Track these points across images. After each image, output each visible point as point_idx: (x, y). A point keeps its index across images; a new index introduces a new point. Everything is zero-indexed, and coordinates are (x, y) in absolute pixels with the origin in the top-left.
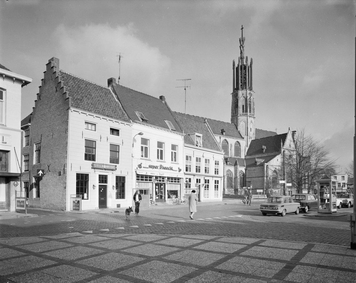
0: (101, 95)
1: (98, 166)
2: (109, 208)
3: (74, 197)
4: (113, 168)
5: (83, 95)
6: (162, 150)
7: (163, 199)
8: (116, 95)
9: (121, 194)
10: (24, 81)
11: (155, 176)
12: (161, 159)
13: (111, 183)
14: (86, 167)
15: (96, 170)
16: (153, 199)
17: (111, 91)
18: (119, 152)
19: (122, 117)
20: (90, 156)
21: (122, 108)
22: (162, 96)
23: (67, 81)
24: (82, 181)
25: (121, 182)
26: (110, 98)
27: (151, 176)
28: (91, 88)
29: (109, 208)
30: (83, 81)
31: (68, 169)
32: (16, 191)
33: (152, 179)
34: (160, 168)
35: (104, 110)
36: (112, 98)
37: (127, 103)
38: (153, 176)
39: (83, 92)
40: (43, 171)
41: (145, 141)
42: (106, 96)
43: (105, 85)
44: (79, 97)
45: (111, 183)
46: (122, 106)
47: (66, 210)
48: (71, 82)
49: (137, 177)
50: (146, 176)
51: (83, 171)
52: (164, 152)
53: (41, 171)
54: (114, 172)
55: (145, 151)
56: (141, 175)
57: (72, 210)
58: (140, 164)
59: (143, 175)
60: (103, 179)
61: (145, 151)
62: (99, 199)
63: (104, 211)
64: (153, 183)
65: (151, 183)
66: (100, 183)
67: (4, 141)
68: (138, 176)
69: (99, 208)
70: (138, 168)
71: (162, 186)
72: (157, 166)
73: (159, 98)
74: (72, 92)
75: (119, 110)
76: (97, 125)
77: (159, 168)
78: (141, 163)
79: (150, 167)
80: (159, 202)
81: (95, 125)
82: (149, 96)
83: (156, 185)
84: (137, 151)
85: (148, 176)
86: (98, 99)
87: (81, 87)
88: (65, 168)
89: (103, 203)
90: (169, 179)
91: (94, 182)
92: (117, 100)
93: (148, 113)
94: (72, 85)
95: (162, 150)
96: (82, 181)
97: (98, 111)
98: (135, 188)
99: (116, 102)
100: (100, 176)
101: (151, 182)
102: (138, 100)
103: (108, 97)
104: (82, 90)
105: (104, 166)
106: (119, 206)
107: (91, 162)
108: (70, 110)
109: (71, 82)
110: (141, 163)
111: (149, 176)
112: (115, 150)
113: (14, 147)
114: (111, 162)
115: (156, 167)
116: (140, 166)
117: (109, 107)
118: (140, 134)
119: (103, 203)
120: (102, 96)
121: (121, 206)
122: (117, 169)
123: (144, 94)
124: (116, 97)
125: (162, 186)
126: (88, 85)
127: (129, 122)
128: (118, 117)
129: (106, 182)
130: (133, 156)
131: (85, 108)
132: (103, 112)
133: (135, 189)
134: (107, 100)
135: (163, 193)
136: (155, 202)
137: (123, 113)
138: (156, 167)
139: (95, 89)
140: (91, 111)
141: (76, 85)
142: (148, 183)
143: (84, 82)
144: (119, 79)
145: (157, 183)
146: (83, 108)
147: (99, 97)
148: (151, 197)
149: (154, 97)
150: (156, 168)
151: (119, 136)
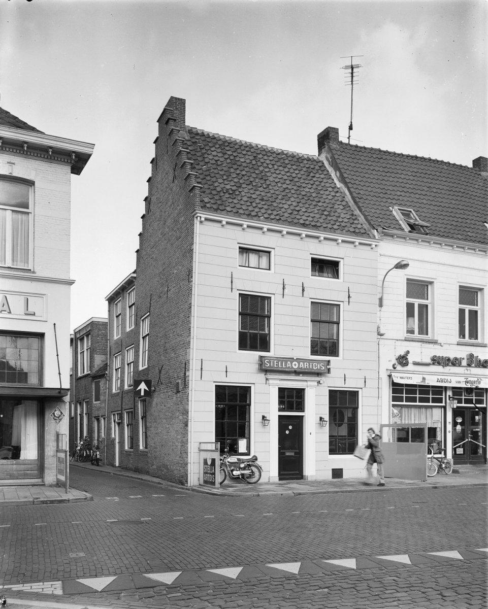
0: (294, 175)
1: (274, 365)
2: (309, 479)
3: (209, 448)
4: (316, 367)
5: (241, 181)
6: (476, 312)
7: (479, 457)
8: (338, 172)
9: (343, 442)
10: (74, 154)
11: (453, 388)
12: (471, 337)
13: (316, 407)
14: (242, 368)
15: (269, 376)
16: (445, 454)
17: (326, 164)
18: (338, 323)
19: (348, 225)
20: (254, 335)
21: (351, 203)
22: (481, 157)
23: (204, 151)
24: (233, 406)
25: (343, 406)
26: (321, 182)
27: (441, 387)
28: (268, 162)
29: (309, 479)
30: (247, 149)
31: (193, 374)
32: (58, 435)
33: (444, 397)
34: (469, 365)
35: (296, 213)
36: (325, 181)
37: (369, 189)
38: (446, 388)
39: (244, 173)
40: (148, 383)
41: (418, 288)
42: (309, 178)
43: (310, 149)
44: (228, 187)
45: (316, 407)
46: (353, 198)
47: (187, 482)
48: (214, 153)
49: (394, 391)
50: (424, 389)
51: (235, 379)
52: (409, 275)
53: (143, 383)
54: (322, 379)
55: (419, 315)
56: (407, 385)
57: (202, 482)
58: (402, 354)
59: (415, 386)
60: (292, 399)
61: (419, 315)
62: (281, 454)
63: (295, 486)
64: (445, 407)
65: (440, 410)
66: (280, 410)
67: (31, 310)
68: (397, 388)
69: (280, 479)
70: (399, 367)
71: (477, 418)
72: (458, 357)
73: (470, 165)
74: (212, 175)
75: (342, 207)
76: (272, 254)
77: (464, 363)
78: (408, 352)
79: (436, 361)
80: (465, 463)
81: (269, 252)
82: (438, 161)
83: (457, 412)
84: (394, 319)
85: (428, 386)
86: (285, 186)
87: (239, 163)
88: (187, 374)
89: (291, 463)
90: (414, 392)
91: (265, 405)
92: (339, 185)
93: (432, 207)
94: (216, 158)
95: (476, 312)
96: (233, 406)
97: (277, 215)
98: (387, 423)
99: (335, 190)
100: (281, 390)
101: (441, 407)
102: (403, 176)
103: (314, 179)
104: (241, 168)
105: (294, 363)
106: (337, 473)
107: (255, 355)
108: (197, 218)
109: (214, 153)
110: (408, 352)
111: (433, 387)
112: (325, 316)
113: (55, 324)
114: (314, 352)
115: (456, 362)
116: (403, 360)
117: (314, 203)
118: (401, 266)
119: (291, 463)
120: (296, 179)
121: (346, 475)
122: (331, 370)
123: (423, 159)
124: (338, 174)
125: (477, 418)
126: (260, 156)
127: (370, 237)
128: (335, 227)
129: (300, 407)
130: (382, 332)
131: (241, 211)
132: (293, 216)
133: (389, 426)
134: (310, 186)
135: (481, 438)
136: (452, 462)
137: (352, 215)
138: (456, 362)
139: (279, 164)
140: (256, 216)
141: (226, 159)
142: (429, 411)
143: (252, 150)
144: (351, 128)
145: (457, 407)
146: (235, 210)
147: (288, 182)
148: (439, 449)
149: (454, 164)
150: (454, 365)
151: (338, 278)
